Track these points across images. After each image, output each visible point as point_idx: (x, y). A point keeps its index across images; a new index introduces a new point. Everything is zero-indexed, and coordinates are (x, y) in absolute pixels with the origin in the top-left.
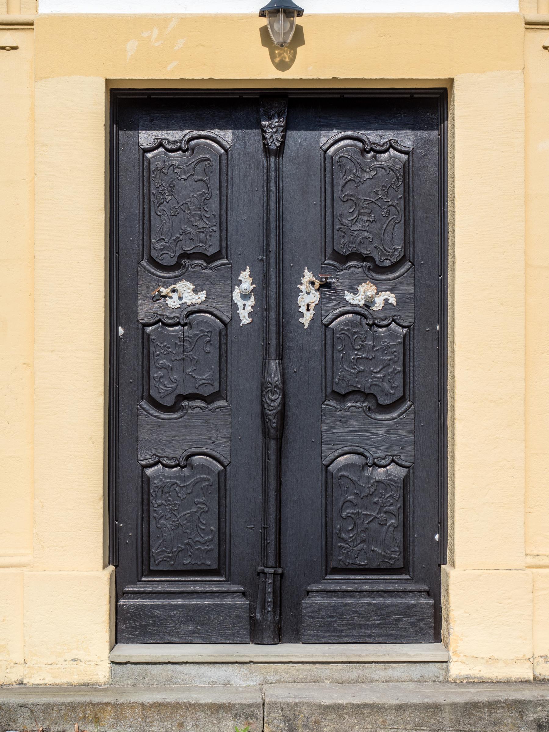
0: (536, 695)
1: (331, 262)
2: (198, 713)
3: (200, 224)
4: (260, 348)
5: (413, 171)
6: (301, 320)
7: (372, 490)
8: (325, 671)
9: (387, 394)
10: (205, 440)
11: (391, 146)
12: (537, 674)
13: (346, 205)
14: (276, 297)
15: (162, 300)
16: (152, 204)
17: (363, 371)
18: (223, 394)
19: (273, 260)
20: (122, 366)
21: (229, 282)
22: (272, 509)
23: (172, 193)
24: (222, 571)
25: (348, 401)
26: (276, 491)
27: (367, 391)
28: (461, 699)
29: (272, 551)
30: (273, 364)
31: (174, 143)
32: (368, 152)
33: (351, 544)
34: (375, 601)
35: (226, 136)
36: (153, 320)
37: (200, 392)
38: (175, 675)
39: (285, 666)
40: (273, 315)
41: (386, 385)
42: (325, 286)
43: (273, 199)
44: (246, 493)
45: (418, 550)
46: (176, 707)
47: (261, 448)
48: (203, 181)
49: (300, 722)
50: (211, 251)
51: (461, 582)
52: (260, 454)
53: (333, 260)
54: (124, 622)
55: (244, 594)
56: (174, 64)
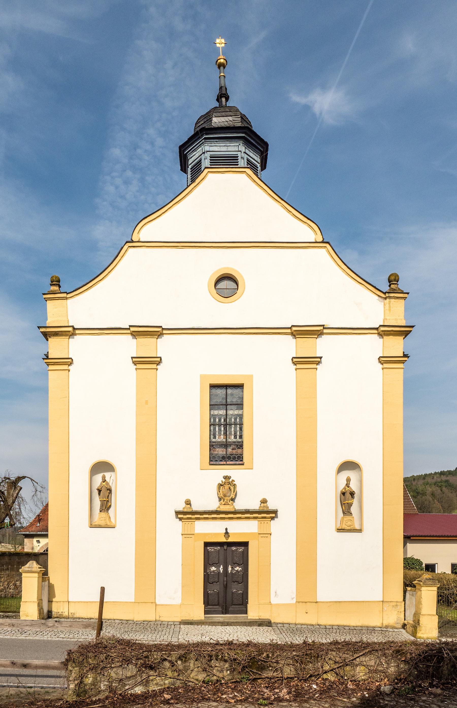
10: (215, 589)
14: (226, 569)
42: (232, 568)
44: (222, 595)
45: (244, 602)
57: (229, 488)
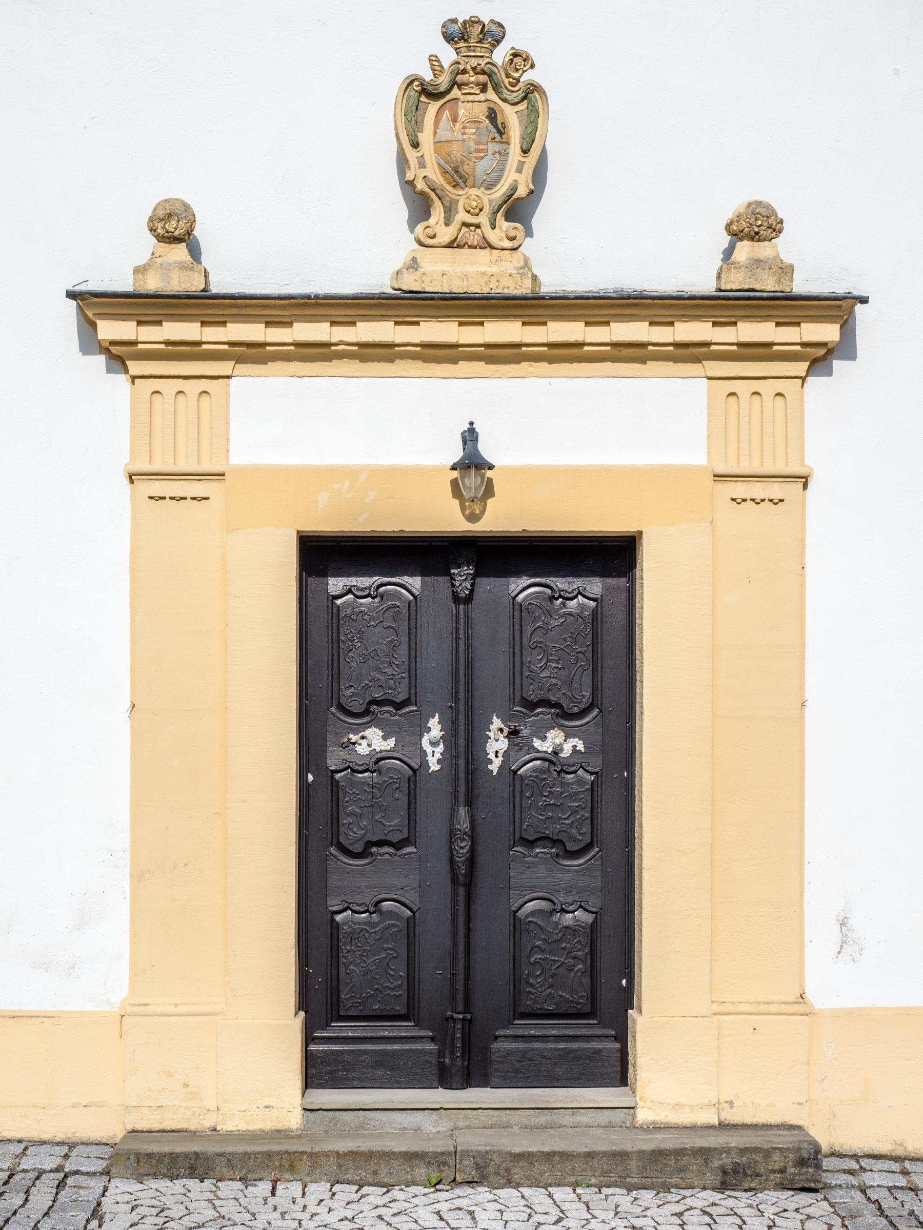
0: (721, 1142)
1: (520, 709)
2: (392, 1161)
3: (389, 670)
4: (449, 795)
5: (602, 619)
6: (489, 767)
7: (560, 936)
8: (514, 1117)
9: (575, 840)
11: (579, 593)
12: (722, 1119)
13: (534, 652)
15: (352, 747)
16: (341, 651)
17: (551, 817)
18: (412, 840)
19: (462, 708)
20: (311, 812)
21: (418, 728)
22: (461, 955)
23: (361, 640)
24: (411, 1016)
25: (537, 847)
26: (465, 937)
27: (555, 837)
28: (647, 1147)
29: (460, 996)
30: (462, 811)
31: (363, 590)
32: (557, 599)
33: (539, 989)
34: (562, 1046)
35: (415, 582)
36: (342, 767)
37: (389, 838)
38: (367, 1121)
39: (475, 1112)
40: (462, 762)
41: (574, 831)
42: (513, 733)
43: (462, 647)
44: (436, 936)
45: (606, 995)
46: (370, 1155)
47: (449, 894)
48: (392, 628)
49: (491, 1169)
50: (400, 698)
51: (645, 1026)
52: (449, 900)
53: (521, 707)
54: (314, 1067)
55: (432, 1039)
57: (492, 116)
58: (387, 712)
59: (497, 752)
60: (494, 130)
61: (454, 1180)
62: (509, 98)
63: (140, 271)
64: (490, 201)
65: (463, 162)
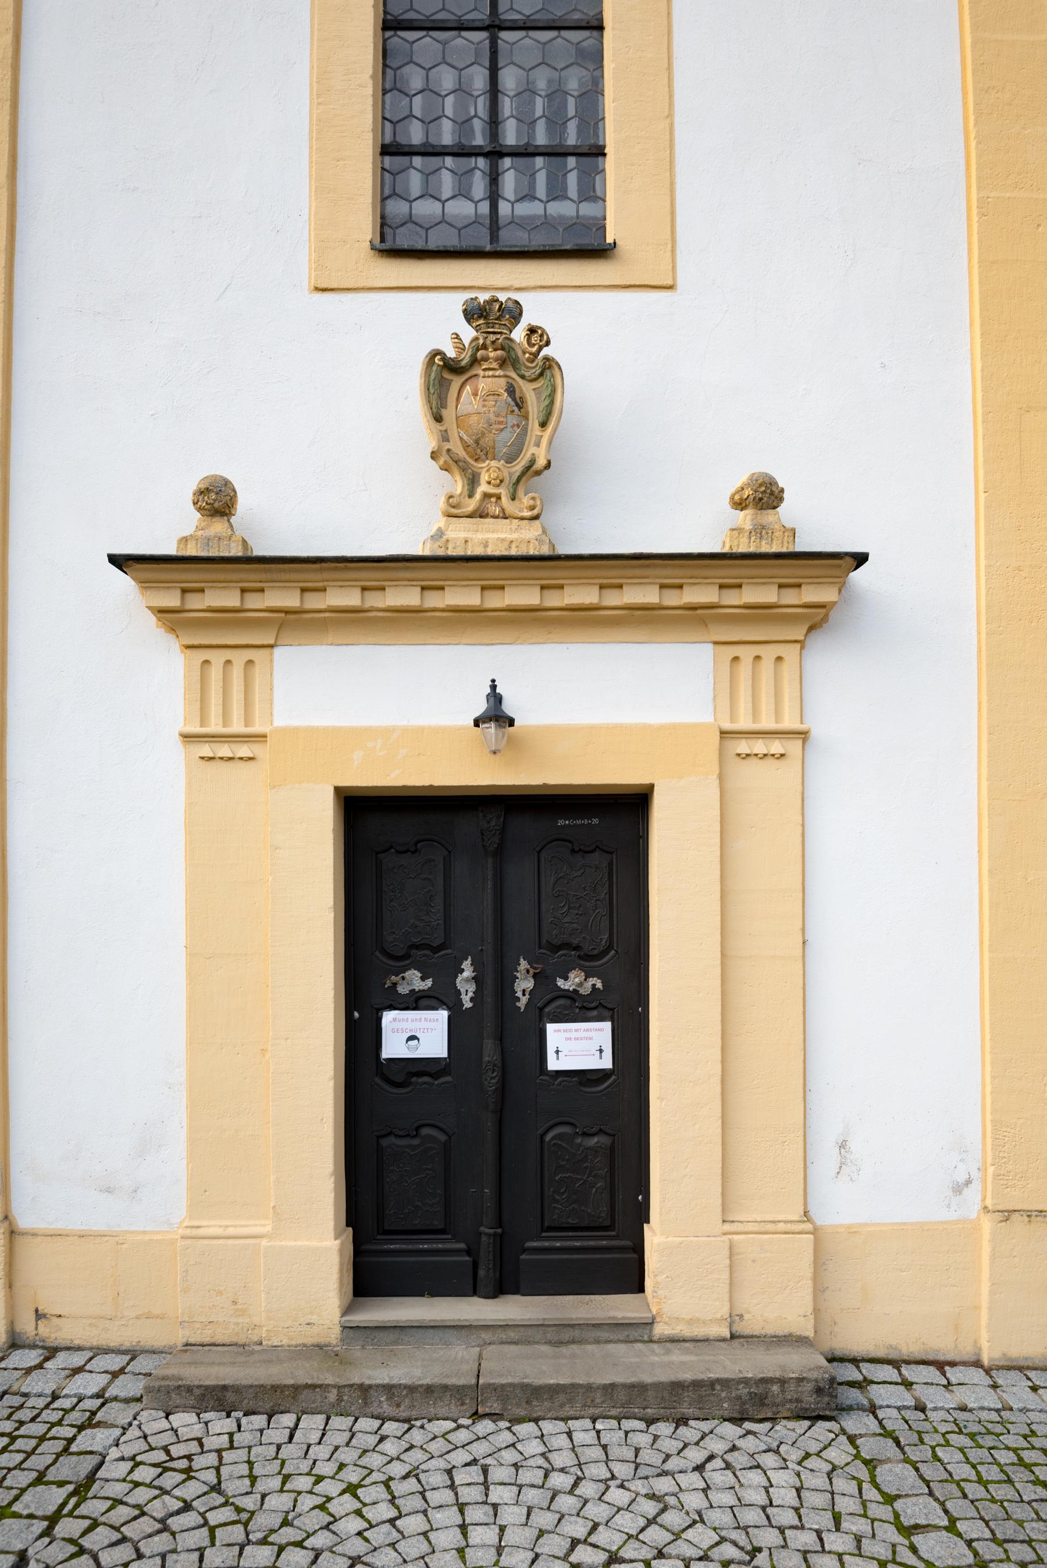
6: (517, 1004)
56: (397, 772)
57: (511, 390)
58: (425, 955)
59: (524, 991)
60: (513, 403)
61: (476, 1413)
62: (527, 374)
63: (184, 540)
64: (511, 475)
65: (483, 434)
